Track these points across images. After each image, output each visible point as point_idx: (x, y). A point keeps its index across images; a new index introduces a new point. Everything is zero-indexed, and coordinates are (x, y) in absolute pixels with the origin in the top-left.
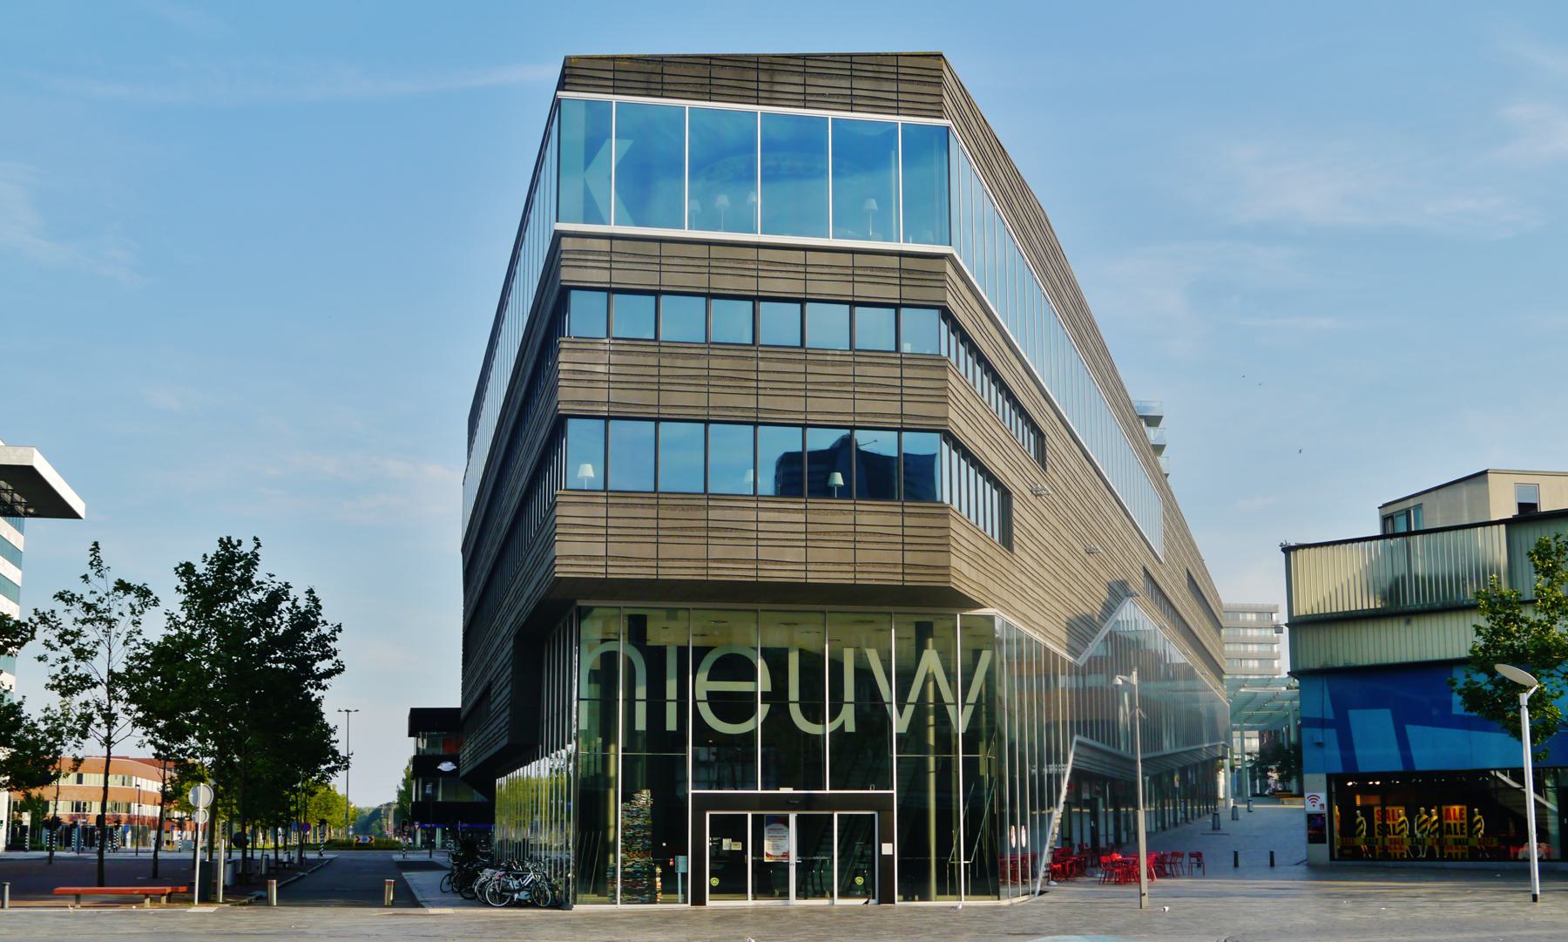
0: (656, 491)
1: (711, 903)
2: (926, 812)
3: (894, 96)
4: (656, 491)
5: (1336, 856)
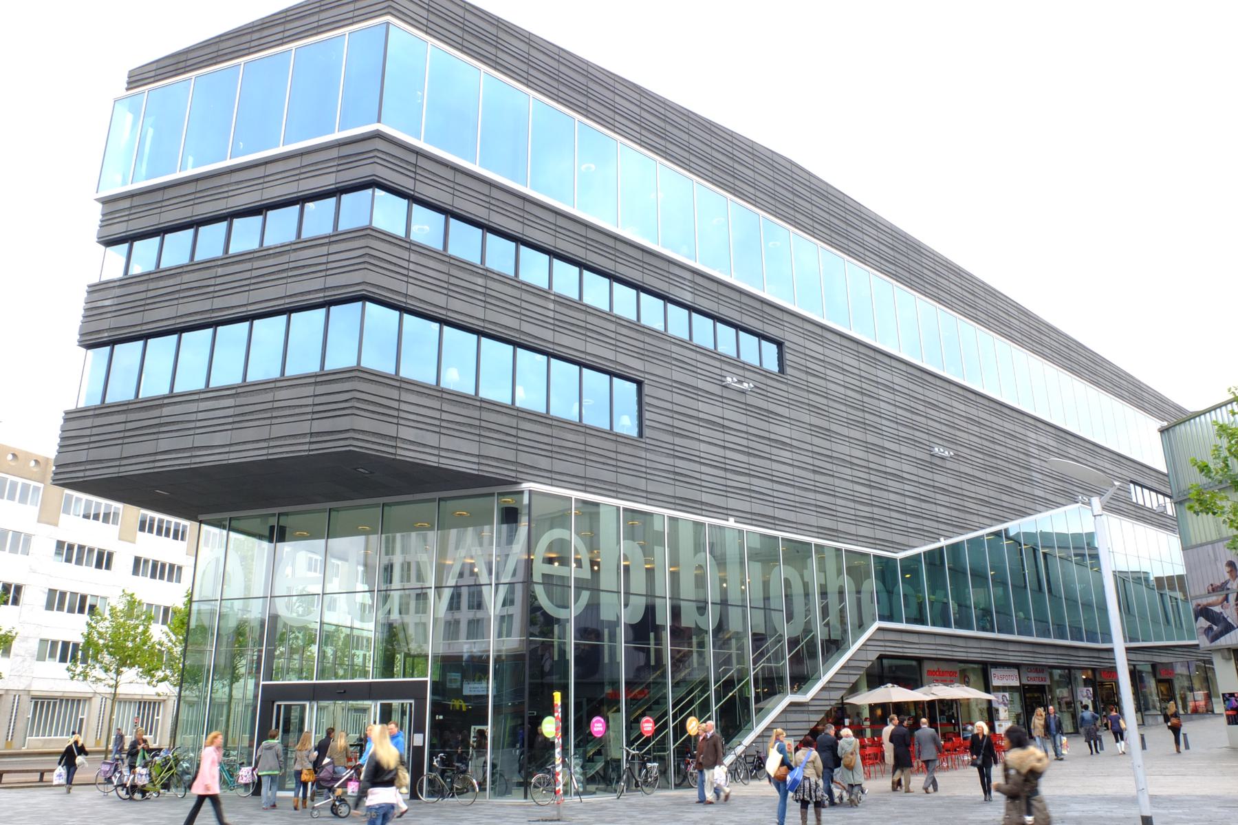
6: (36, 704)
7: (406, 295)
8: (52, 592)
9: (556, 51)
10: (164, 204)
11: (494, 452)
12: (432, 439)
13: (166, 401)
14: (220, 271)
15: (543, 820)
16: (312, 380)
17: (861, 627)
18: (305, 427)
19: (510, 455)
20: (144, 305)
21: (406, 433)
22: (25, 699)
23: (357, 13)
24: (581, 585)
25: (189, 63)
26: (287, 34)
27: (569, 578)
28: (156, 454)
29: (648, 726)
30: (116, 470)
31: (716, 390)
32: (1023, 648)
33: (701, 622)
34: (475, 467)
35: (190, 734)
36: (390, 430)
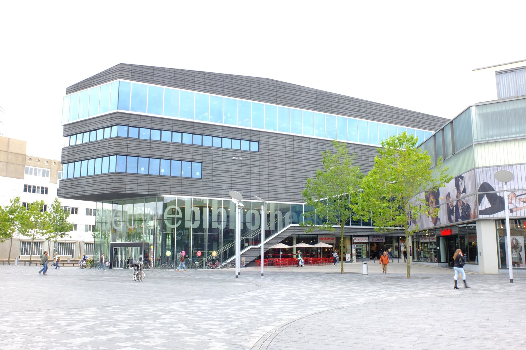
0: (126, 172)
1: (130, 268)
2: (176, 248)
3: (250, 96)
4: (126, 172)
5: (500, 267)
6: (86, 245)
7: (127, 152)
8: (87, 209)
9: (174, 70)
10: (76, 127)
11: (153, 188)
12: (135, 187)
13: (79, 179)
14: (88, 146)
15: (10, 250)
16: (106, 175)
17: (284, 226)
18: (105, 187)
19: (158, 188)
20: (73, 154)
21: (128, 186)
22: (83, 244)
23: (113, 76)
24: (178, 219)
25: (79, 87)
26: (99, 81)
27: (175, 218)
28: (78, 191)
29: (199, 253)
30: (70, 195)
31: (230, 161)
32: (365, 230)
33: (219, 227)
34: (148, 192)
35: (92, 255)
36: (124, 186)
